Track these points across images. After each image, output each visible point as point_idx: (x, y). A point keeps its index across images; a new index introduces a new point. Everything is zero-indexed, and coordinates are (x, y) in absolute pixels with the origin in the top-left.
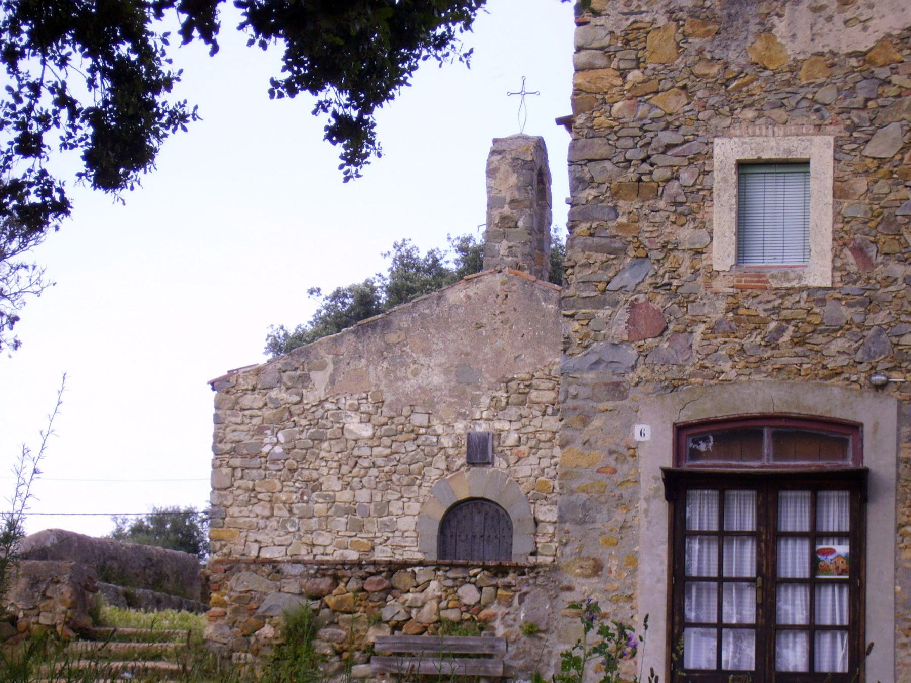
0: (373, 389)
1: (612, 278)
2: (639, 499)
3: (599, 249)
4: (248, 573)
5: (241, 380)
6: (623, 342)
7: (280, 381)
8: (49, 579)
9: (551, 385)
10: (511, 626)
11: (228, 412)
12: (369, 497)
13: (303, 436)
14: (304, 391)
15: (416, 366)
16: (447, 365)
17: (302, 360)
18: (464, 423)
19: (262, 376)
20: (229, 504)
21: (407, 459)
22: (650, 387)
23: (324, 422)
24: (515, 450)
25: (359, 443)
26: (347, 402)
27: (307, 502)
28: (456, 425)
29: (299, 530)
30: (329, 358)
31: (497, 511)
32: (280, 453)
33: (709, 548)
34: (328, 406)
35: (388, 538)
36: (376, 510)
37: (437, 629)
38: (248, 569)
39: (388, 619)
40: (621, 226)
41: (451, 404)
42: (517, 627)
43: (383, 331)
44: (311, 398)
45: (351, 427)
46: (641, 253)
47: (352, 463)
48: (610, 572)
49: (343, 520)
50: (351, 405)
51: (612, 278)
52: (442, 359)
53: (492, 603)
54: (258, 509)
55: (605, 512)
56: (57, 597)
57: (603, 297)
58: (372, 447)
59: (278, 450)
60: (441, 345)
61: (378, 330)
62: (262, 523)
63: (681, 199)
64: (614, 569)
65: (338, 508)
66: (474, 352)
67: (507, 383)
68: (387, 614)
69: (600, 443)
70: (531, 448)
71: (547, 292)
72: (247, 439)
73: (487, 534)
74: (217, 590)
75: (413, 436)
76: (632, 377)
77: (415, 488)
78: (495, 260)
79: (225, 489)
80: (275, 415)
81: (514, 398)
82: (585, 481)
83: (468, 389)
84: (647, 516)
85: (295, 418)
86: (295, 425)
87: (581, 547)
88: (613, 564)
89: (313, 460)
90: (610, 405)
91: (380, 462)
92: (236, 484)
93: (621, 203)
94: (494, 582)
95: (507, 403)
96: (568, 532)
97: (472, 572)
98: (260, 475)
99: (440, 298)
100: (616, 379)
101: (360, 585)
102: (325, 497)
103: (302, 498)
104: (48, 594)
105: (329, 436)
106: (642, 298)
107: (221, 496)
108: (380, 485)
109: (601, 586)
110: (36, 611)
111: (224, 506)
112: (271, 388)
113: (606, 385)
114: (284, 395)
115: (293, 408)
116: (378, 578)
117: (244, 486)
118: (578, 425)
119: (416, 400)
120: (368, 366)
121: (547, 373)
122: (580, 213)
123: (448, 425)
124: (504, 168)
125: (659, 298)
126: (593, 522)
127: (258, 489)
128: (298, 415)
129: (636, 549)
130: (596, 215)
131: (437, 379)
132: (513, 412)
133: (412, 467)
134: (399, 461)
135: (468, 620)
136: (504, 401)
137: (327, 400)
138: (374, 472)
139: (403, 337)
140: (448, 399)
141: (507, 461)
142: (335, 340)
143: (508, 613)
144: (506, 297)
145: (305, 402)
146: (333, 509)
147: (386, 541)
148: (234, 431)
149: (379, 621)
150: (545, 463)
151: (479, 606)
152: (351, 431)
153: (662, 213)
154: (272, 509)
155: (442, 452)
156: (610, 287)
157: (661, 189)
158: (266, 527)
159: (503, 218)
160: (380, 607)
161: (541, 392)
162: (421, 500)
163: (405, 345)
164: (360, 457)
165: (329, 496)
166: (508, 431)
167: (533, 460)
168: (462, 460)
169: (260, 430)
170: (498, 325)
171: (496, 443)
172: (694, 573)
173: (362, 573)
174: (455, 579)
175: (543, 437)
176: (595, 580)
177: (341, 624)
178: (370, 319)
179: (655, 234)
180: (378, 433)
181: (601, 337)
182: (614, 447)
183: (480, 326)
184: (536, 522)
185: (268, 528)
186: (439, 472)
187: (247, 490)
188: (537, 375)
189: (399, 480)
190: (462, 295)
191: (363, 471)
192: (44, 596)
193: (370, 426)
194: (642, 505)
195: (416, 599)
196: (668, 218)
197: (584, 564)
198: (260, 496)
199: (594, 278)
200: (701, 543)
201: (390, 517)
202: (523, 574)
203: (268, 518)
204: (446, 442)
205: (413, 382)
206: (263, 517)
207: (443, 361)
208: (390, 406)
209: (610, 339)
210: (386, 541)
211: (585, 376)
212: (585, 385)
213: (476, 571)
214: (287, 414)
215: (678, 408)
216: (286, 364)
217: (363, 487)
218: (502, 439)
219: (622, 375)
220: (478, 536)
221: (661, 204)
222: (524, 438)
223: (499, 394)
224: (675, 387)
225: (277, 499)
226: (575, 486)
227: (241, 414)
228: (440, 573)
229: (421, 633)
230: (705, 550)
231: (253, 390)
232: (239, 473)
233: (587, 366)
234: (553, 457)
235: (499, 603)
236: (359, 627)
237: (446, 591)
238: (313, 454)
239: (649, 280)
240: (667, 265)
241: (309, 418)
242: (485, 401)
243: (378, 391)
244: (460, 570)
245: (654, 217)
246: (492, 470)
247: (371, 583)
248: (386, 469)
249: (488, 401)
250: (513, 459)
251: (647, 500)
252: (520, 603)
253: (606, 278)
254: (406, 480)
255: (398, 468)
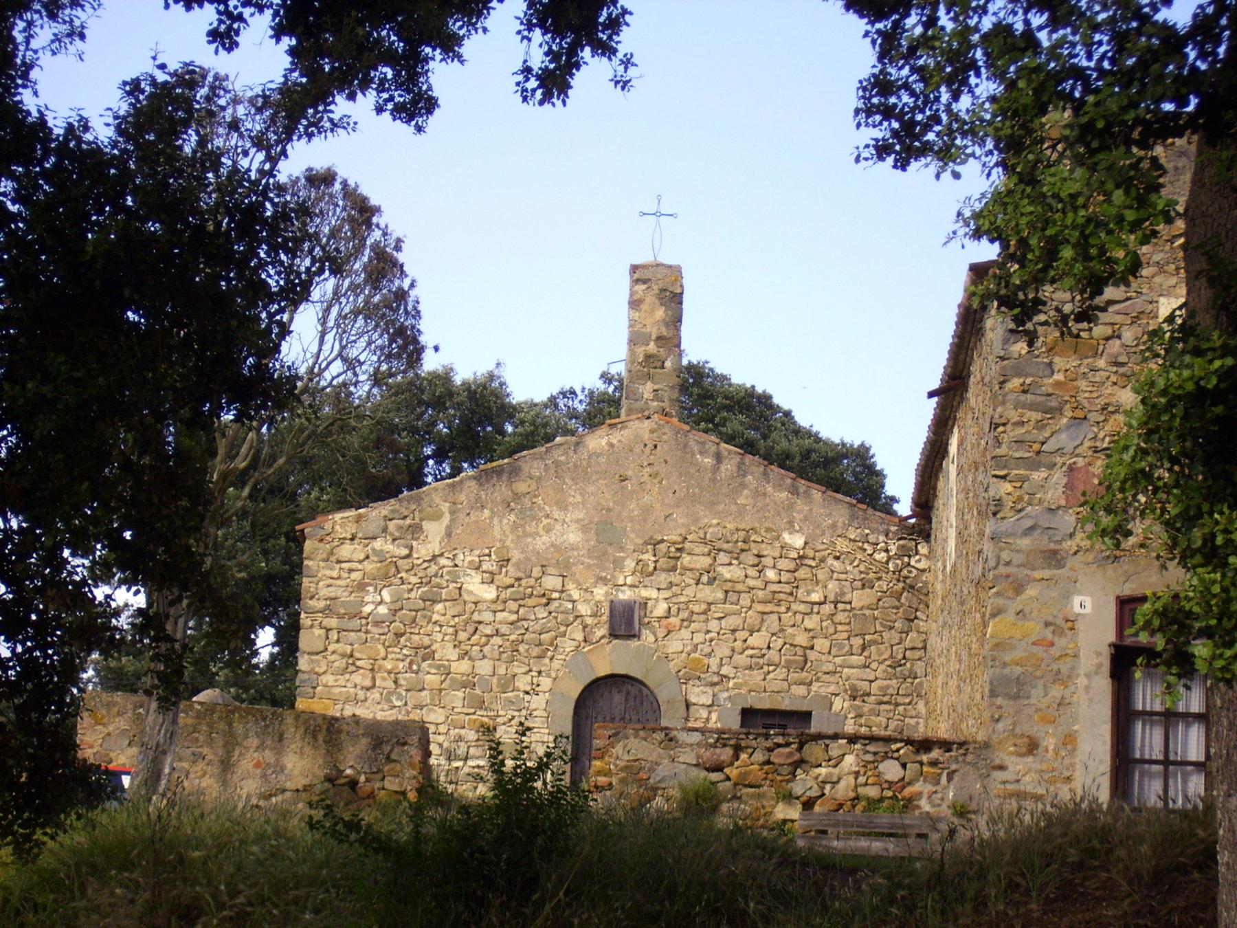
0: (498, 545)
1: (1047, 439)
2: (1078, 675)
3: (1033, 407)
4: (637, 741)
5: (338, 527)
6: (1059, 508)
7: (385, 530)
8: (395, 740)
9: (706, 550)
10: (939, 805)
11: (322, 564)
12: (491, 669)
13: (413, 595)
14: (414, 543)
15: (548, 521)
16: (586, 522)
17: (414, 507)
18: (605, 588)
19: (363, 524)
20: (322, 671)
21: (538, 627)
22: (1090, 557)
23: (438, 580)
24: (664, 622)
25: (480, 606)
26: (465, 558)
27: (417, 673)
28: (595, 590)
29: (406, 704)
30: (445, 507)
31: (640, 690)
32: (385, 615)
33: (1151, 729)
34: (443, 561)
35: (513, 717)
36: (499, 685)
37: (854, 806)
38: (636, 736)
39: (799, 793)
40: (1058, 384)
41: (589, 566)
42: (944, 807)
43: (510, 478)
44: (423, 551)
45: (471, 587)
46: (1080, 414)
47: (470, 629)
48: (1047, 751)
49: (460, 694)
50: (471, 562)
51: (1047, 439)
52: (580, 515)
53: (918, 780)
54: (357, 678)
55: (1040, 687)
56: (405, 759)
57: (1037, 459)
58: (495, 612)
59: (383, 610)
60: (579, 499)
61: (505, 477)
62: (361, 695)
63: (1123, 359)
64: (1051, 747)
65: (454, 681)
66: (618, 508)
67: (655, 545)
68: (798, 789)
69: (1035, 613)
70: (683, 620)
71: (703, 443)
72: (344, 597)
73: (628, 717)
74: (601, 758)
75: (544, 601)
76: (1070, 545)
77: (547, 661)
78: (640, 404)
79: (317, 654)
80: (379, 569)
81: (663, 562)
82: (1018, 654)
83: (610, 550)
84: (1087, 692)
85: (403, 574)
86: (403, 583)
87: (1014, 724)
88: (1050, 743)
89: (424, 624)
90: (1046, 573)
91: (504, 629)
92: (331, 648)
93: (1057, 360)
94: (919, 758)
95: (655, 568)
96: (1000, 707)
97: (894, 747)
98: (360, 638)
99: (578, 444)
100: (1052, 546)
101: (766, 758)
102: (438, 667)
103: (410, 667)
104: (393, 756)
105: (444, 597)
106: (1081, 462)
107: (312, 661)
108: (504, 656)
109: (1037, 766)
110: (380, 776)
111: (316, 673)
112: (375, 538)
113: (1042, 552)
114: (389, 547)
115: (400, 563)
116: (787, 750)
117: (340, 651)
118: (1010, 593)
119: (547, 559)
120: (491, 518)
121: (702, 535)
122: (1012, 367)
123: (586, 590)
124: (650, 299)
125: (1099, 463)
126: (1028, 698)
127: (357, 655)
128: (407, 571)
129: (1076, 728)
130: (1031, 371)
131: (574, 537)
132: (662, 578)
133: (543, 636)
134: (527, 629)
135: (891, 798)
136: (652, 566)
137: (442, 555)
138: (497, 640)
139: (534, 486)
140: (587, 560)
141: (655, 634)
142: (453, 486)
143: (935, 792)
144: (656, 447)
145: (415, 555)
146: (448, 681)
147: (510, 720)
148: (329, 586)
149: (789, 797)
150: (699, 638)
151: (903, 783)
152: (471, 593)
153: (1102, 373)
154: (374, 679)
155: (579, 621)
156: (1044, 448)
157: (1101, 348)
158: (366, 700)
159: (648, 357)
160: (788, 781)
161: (695, 558)
162: (553, 675)
163: (536, 496)
164: (480, 623)
165: (443, 666)
166: (657, 600)
167: (685, 634)
168: (602, 631)
169: (361, 587)
170: (646, 478)
171: (642, 614)
172: (1138, 756)
173: (769, 744)
174: (875, 754)
175: (697, 608)
176: (1030, 759)
177: (744, 798)
178: (494, 464)
179: (1095, 395)
180: (503, 596)
181: (1036, 501)
182: (1050, 619)
183: (624, 479)
184: (688, 705)
185: (369, 701)
186: (575, 643)
187: (343, 655)
188: (690, 537)
189: (527, 651)
190: (604, 442)
191: (484, 640)
192: (388, 758)
193: (493, 589)
194: (1082, 681)
195: (831, 774)
196: (1108, 378)
197: (1019, 741)
198: (359, 663)
199: (1028, 438)
200: (1144, 725)
201: (515, 693)
202: (949, 750)
203: (368, 689)
204: (584, 609)
205: (545, 538)
206: (362, 688)
207: (581, 516)
208: (517, 565)
209: (1046, 504)
210: (510, 720)
211: (1019, 541)
212: (1018, 551)
213: (899, 745)
214: (393, 569)
215: (1121, 580)
216: (393, 511)
217: (484, 657)
218: (649, 609)
219: (1060, 542)
220: (618, 718)
221: (1101, 363)
222: (674, 610)
223: (645, 557)
224: (1116, 557)
225: (380, 667)
226: (1008, 657)
227: (338, 566)
228: (858, 746)
229: (837, 810)
230: (1147, 731)
231: (352, 539)
232: (334, 635)
233: (1020, 531)
234: (708, 632)
235: (925, 781)
236: (765, 803)
237: (865, 766)
238: (425, 617)
239: (1087, 444)
240: (1108, 428)
241: (420, 575)
242: (630, 564)
243: (503, 547)
244: (880, 743)
245: (1094, 376)
246: (638, 643)
247: (780, 755)
248: (513, 637)
249: (633, 564)
250: (661, 633)
251: (1088, 676)
252: (948, 782)
253: (1041, 438)
254: (536, 651)
255: (526, 637)
